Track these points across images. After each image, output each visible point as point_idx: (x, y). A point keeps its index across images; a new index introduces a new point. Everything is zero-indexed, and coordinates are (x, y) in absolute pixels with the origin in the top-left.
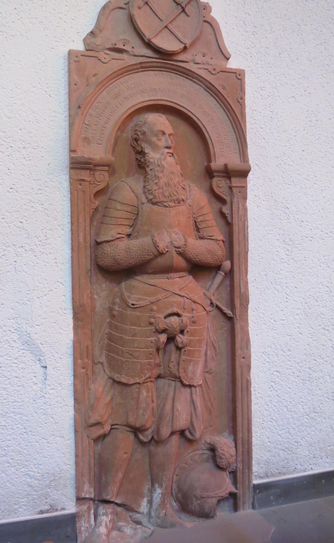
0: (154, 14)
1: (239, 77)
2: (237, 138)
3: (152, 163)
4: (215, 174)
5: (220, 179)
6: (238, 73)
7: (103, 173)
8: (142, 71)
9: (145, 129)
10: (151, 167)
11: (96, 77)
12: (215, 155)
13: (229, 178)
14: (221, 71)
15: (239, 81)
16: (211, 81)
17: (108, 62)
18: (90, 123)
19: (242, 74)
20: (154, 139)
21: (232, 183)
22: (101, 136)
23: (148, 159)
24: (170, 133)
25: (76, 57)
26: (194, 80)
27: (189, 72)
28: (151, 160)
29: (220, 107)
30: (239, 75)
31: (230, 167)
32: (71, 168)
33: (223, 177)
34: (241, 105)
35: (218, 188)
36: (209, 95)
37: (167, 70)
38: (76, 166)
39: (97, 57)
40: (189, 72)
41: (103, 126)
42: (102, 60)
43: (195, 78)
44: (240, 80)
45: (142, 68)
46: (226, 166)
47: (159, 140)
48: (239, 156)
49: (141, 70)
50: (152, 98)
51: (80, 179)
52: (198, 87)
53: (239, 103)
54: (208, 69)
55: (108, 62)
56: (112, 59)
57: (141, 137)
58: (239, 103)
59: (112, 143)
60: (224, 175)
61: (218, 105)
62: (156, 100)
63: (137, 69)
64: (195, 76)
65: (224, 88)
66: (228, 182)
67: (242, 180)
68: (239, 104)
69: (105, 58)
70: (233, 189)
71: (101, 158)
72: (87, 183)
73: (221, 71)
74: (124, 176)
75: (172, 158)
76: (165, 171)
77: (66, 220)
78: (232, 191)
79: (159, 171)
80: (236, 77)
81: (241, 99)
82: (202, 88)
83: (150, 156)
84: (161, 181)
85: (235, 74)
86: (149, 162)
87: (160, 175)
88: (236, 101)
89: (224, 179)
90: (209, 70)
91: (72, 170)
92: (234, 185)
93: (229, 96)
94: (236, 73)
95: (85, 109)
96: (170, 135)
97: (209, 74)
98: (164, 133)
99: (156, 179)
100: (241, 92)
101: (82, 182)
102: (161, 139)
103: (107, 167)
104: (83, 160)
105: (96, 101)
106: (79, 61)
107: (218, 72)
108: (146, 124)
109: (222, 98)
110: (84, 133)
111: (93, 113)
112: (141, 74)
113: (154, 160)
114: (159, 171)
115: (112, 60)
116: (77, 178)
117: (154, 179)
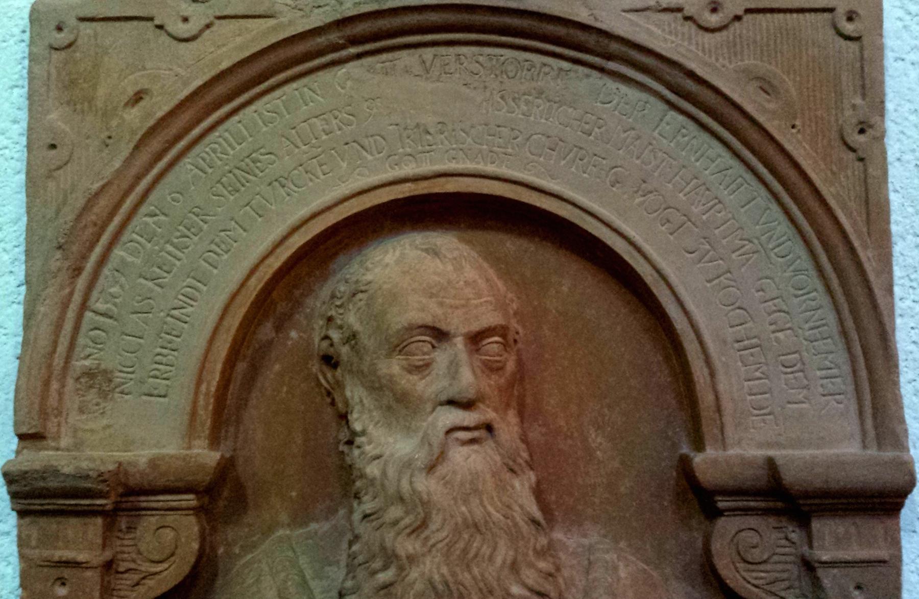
0: (240, 13)
1: (849, 28)
2: (841, 321)
3: (372, 481)
4: (721, 505)
5: (752, 521)
6: (841, 11)
7: (171, 518)
8: (359, 56)
9: (352, 319)
10: (368, 506)
11: (142, 104)
12: (719, 409)
13: (802, 519)
14: (219, 18)
15: (853, 46)
16: (692, 66)
17: (201, 32)
18: (115, 305)
19: (860, 12)
20: (393, 367)
21: (815, 544)
22: (164, 360)
23: (359, 464)
24: (475, 327)
25: (59, 29)
26: (612, 65)
27: (581, 36)
28: (373, 470)
29: (749, 176)
30: (850, 19)
31: (789, 476)
32: (22, 514)
33: (766, 512)
34: (861, 160)
35: (741, 565)
36: (691, 126)
37: (473, 36)
38: (36, 504)
39: (151, 19)
40: (581, 36)
41: (175, 313)
42: (170, 28)
43: (609, 57)
44: (858, 39)
45: (354, 41)
46: (771, 463)
47: (422, 369)
48: (853, 407)
49: (353, 50)
50: (409, 169)
51: (56, 558)
52: (633, 94)
53: (853, 150)
54: (679, 10)
55: (201, 32)
56: (219, 18)
57: (345, 350)
58: (853, 150)
59: (213, 389)
60: (771, 504)
61: (738, 168)
62: (425, 178)
63: (335, 48)
64: (614, 47)
65: (767, 87)
66: (793, 536)
67: (876, 527)
68: (852, 155)
69: (186, 20)
70: (820, 573)
71: (153, 463)
72: (89, 574)
73: (748, 11)
74: (284, 517)
75: (491, 443)
76: (436, 521)
77: (569, 219)
78: (816, 583)
79: (402, 524)
80: (833, 32)
81: (862, 131)
82: (652, 99)
83: (368, 448)
84: (414, 574)
85: (826, 15)
86: (362, 476)
87: (407, 546)
88: (837, 143)
89: (772, 521)
90: (689, 10)
91: (27, 520)
92: (825, 558)
93: (798, 123)
94: (831, 10)
95: (91, 248)
96: (476, 339)
97: (689, 27)
98: (440, 335)
99: (385, 568)
100: (864, 96)
101: (66, 573)
102: (427, 365)
103: (191, 496)
104: (53, 484)
105: (144, 209)
106: (70, 45)
107: (738, 18)
108: (360, 296)
109: (754, 136)
110: (88, 351)
111: (130, 259)
112: (352, 68)
113: (384, 473)
114: (402, 524)
115: (217, 22)
116: (46, 553)
117: (377, 564)
